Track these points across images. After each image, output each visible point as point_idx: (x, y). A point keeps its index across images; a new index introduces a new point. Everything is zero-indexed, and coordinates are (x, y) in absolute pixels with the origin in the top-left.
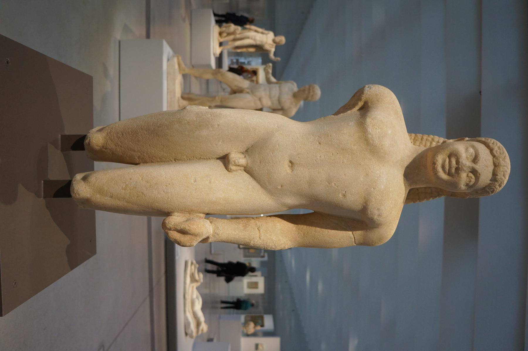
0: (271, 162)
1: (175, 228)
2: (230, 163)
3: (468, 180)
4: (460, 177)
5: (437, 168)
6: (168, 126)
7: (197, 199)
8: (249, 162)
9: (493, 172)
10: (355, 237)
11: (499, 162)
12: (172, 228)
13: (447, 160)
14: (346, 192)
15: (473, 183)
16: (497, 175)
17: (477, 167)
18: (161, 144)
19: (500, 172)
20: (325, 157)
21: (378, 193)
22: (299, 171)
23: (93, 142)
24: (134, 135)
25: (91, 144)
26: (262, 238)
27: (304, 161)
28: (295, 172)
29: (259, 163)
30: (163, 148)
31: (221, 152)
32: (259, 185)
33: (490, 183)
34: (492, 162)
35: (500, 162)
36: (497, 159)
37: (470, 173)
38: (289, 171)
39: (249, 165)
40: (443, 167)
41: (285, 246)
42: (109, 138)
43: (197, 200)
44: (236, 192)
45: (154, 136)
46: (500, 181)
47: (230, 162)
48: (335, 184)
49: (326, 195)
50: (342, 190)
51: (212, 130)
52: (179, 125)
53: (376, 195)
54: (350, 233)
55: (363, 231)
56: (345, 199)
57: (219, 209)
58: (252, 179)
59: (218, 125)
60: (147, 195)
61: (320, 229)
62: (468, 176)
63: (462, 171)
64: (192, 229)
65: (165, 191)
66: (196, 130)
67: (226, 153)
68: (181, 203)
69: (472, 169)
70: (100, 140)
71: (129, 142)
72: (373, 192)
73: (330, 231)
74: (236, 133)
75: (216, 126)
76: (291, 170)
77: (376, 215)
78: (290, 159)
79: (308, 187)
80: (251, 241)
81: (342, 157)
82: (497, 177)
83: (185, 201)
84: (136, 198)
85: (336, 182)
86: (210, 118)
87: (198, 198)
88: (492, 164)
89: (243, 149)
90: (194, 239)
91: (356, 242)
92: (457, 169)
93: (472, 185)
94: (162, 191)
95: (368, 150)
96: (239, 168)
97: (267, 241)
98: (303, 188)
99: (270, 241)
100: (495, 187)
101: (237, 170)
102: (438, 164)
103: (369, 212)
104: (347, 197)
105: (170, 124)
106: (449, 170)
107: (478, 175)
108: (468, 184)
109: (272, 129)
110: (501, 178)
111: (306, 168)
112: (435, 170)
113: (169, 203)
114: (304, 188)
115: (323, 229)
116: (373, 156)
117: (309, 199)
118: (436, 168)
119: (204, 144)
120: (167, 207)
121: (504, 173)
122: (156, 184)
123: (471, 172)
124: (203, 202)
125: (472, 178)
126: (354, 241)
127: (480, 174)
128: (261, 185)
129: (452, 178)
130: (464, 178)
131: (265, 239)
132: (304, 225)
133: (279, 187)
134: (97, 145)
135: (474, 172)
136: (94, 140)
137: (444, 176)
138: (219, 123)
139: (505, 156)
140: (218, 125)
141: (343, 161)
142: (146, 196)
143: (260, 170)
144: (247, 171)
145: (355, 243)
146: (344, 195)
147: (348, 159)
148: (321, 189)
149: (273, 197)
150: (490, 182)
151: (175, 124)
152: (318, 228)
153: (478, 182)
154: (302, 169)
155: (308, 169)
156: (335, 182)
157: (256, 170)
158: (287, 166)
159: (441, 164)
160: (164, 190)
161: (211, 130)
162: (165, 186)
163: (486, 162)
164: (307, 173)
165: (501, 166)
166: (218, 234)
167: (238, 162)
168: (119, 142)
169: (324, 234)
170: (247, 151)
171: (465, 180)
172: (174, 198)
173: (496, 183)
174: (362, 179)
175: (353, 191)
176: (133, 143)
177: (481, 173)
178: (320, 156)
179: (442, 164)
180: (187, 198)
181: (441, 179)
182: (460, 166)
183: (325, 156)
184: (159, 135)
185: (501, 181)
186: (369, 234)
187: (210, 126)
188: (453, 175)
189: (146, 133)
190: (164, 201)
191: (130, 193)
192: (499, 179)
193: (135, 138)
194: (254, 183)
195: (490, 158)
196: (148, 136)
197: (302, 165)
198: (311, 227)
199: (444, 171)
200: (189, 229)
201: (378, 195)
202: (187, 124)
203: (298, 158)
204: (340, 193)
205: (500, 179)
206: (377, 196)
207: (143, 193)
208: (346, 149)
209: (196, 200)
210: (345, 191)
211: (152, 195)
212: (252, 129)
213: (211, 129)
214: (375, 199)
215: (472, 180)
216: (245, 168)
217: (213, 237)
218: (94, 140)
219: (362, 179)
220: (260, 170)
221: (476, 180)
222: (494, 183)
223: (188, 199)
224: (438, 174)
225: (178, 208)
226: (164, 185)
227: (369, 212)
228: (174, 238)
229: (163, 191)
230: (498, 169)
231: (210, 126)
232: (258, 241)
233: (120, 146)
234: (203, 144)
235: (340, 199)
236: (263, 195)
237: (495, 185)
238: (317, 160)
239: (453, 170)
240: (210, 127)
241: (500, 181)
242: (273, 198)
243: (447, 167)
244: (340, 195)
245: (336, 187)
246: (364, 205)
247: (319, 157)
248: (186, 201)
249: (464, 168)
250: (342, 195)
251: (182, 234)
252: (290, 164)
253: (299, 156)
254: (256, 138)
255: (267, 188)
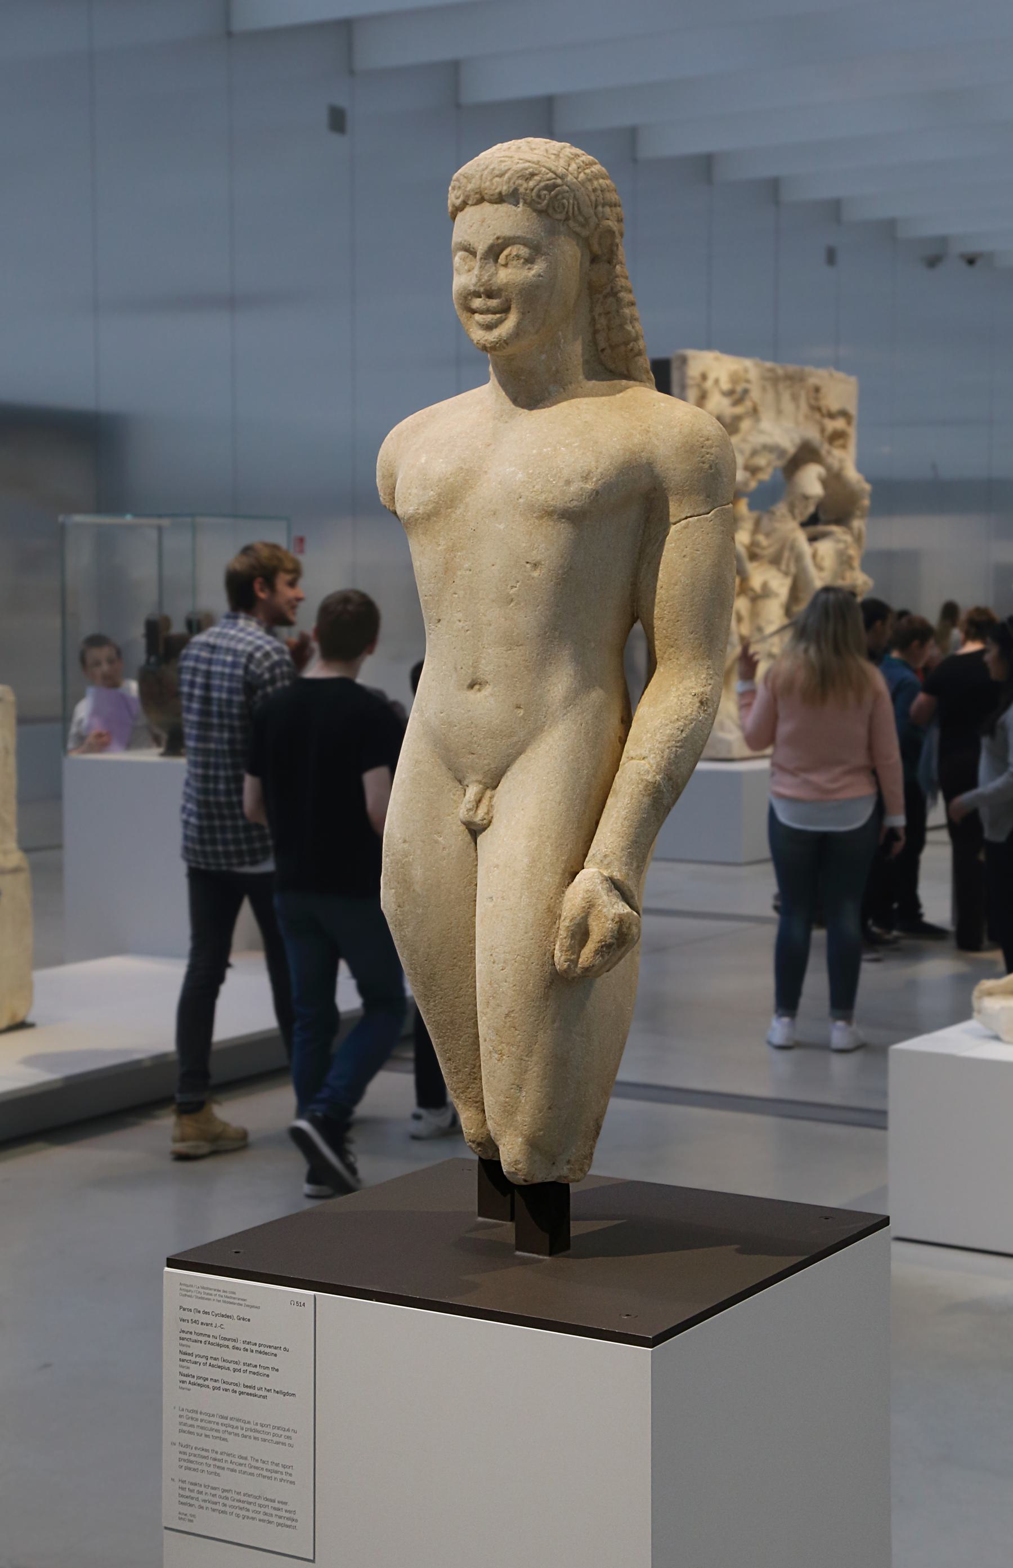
0: (470, 730)
1: (569, 950)
2: (471, 820)
3: (515, 262)
4: (507, 284)
5: (492, 342)
6: (411, 951)
7: (521, 897)
8: (474, 778)
9: (496, 203)
10: (684, 516)
11: (472, 193)
12: (569, 957)
13: (477, 317)
14: (528, 563)
15: (522, 247)
16: (500, 193)
17: (481, 248)
18: (450, 972)
19: (494, 187)
20: (460, 611)
21: (530, 487)
22: (486, 669)
23: (474, 1134)
24: (443, 1033)
25: (479, 1140)
26: (644, 754)
27: (468, 657)
28: (489, 677)
29: (474, 756)
30: (460, 968)
31: (460, 839)
32: (520, 758)
33: (525, 202)
34: (476, 206)
35: (473, 190)
36: (468, 197)
37: (499, 260)
38: (487, 690)
39: (480, 778)
40: (489, 327)
41: (691, 694)
42: (462, 1093)
43: (524, 897)
44: (523, 809)
45: (435, 986)
46: (514, 183)
47: (469, 820)
48: (512, 587)
49: (538, 606)
50: (525, 571)
51: (414, 855)
52: (406, 926)
53: (532, 492)
54: (673, 529)
55: (670, 498)
56: (543, 563)
57: (551, 850)
58: (509, 773)
59: (405, 841)
60: (509, 1005)
61: (656, 608)
62: (506, 265)
63: (491, 282)
64: (571, 913)
65: (503, 967)
66: (414, 890)
67: (463, 828)
68: (526, 933)
69: (485, 259)
70: (470, 1115)
71: (459, 1044)
72: (527, 500)
73: (659, 584)
74: (423, 804)
75: (406, 845)
76: (486, 685)
77: (583, 486)
78: (465, 687)
79: (521, 647)
80: (642, 780)
81: (459, 573)
82: (504, 194)
83: (524, 923)
84: (517, 1032)
85: (507, 586)
86: (391, 857)
87: (519, 895)
88: (478, 207)
89: (457, 790)
90: (599, 911)
91: (707, 510)
92: (490, 295)
93: (530, 248)
94: (502, 971)
95: (447, 514)
96: (485, 802)
97: (657, 740)
98: (523, 658)
99: (658, 734)
100: (532, 190)
101: (491, 807)
102: (484, 339)
103: (574, 504)
104: (539, 558)
105: (407, 947)
106: (494, 313)
107: (500, 241)
108: (525, 259)
109: (420, 724)
110: (506, 182)
111: (481, 653)
112: (498, 345)
113: (527, 960)
114: (522, 656)
115: (657, 601)
116: (460, 500)
117: (555, 643)
118: (492, 345)
119: (443, 875)
120: (538, 964)
121: (497, 176)
122: (490, 984)
123: (496, 260)
124: (531, 884)
125: (510, 254)
126: (696, 518)
127: (498, 238)
128: (519, 753)
129: (512, 303)
130: (510, 274)
131: (649, 746)
132: (654, 645)
133: (521, 712)
134: (480, 1126)
135: (494, 252)
136: (470, 1131)
137: (511, 321)
138: (400, 839)
139: (463, 175)
140: (404, 842)
141: (467, 570)
142: (512, 1009)
143: (488, 754)
144: (495, 784)
145: (708, 513)
146: (535, 565)
147: (464, 560)
148: (526, 617)
149: (546, 727)
150: (521, 205)
151: (404, 936)
152: (655, 612)
153: (518, 237)
154: (483, 661)
155: (484, 647)
156: (509, 587)
157: (489, 764)
158: (479, 695)
159: (484, 331)
160: (501, 968)
161: (413, 859)
162: (494, 965)
163: (474, 223)
164: (490, 651)
165: (480, 188)
166: (605, 856)
167: (470, 802)
168: (466, 1069)
169: (665, 599)
170: (460, 782)
171: (514, 270)
172: (515, 947)
173: (522, 190)
174: (502, 527)
175: (525, 546)
176: (461, 1037)
177: (495, 234)
178: (458, 622)
179: (484, 330)
180: (518, 919)
181: (519, 324)
182: (482, 289)
183: (459, 610)
184: (431, 974)
185: (516, 178)
186: (673, 482)
187: (405, 860)
188: (507, 300)
189: (433, 1003)
190: (523, 970)
191: (508, 1044)
192: (509, 187)
193: (448, 1029)
194: (515, 768)
195: (469, 210)
196: (437, 998)
197: (476, 662)
198: (655, 629)
199: (501, 321)
200: (569, 920)
201: (534, 487)
202: (402, 909)
203: (462, 670)
204: (530, 576)
205: (509, 182)
206: (535, 489)
207: (507, 1015)
208: (446, 564)
209: (522, 899)
210: (525, 564)
211: (509, 995)
212: (416, 768)
213: (412, 857)
214: (542, 492)
215: (515, 254)
216: (488, 788)
217: (610, 867)
218: (470, 1131)
219: (502, 527)
220: (488, 754)
221: (514, 244)
222: (521, 194)
223: (519, 917)
224: (505, 339)
225: (541, 941)
226: (493, 968)
227: (575, 503)
228: (592, 955)
229: (503, 970)
230: (486, 193)
231: (405, 860)
232: (649, 763)
233: (473, 1069)
234: (442, 878)
235: (543, 574)
236: (539, 749)
237: (528, 191)
238: (467, 628)
239: (494, 303)
240: (407, 859)
241: (514, 183)
242: (550, 727)
243: (489, 318)
244: (536, 574)
245: (518, 584)
246: (556, 517)
247: (461, 624)
248: (522, 922)
249: (483, 280)
250: (535, 570)
251: (589, 938)
252: (477, 687)
253: (460, 667)
254: (433, 760)
255: (524, 741)
